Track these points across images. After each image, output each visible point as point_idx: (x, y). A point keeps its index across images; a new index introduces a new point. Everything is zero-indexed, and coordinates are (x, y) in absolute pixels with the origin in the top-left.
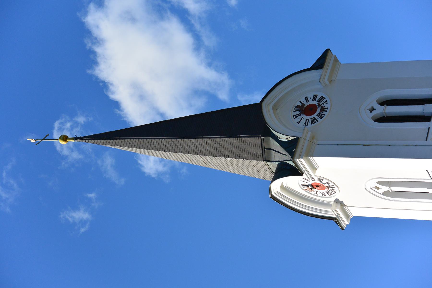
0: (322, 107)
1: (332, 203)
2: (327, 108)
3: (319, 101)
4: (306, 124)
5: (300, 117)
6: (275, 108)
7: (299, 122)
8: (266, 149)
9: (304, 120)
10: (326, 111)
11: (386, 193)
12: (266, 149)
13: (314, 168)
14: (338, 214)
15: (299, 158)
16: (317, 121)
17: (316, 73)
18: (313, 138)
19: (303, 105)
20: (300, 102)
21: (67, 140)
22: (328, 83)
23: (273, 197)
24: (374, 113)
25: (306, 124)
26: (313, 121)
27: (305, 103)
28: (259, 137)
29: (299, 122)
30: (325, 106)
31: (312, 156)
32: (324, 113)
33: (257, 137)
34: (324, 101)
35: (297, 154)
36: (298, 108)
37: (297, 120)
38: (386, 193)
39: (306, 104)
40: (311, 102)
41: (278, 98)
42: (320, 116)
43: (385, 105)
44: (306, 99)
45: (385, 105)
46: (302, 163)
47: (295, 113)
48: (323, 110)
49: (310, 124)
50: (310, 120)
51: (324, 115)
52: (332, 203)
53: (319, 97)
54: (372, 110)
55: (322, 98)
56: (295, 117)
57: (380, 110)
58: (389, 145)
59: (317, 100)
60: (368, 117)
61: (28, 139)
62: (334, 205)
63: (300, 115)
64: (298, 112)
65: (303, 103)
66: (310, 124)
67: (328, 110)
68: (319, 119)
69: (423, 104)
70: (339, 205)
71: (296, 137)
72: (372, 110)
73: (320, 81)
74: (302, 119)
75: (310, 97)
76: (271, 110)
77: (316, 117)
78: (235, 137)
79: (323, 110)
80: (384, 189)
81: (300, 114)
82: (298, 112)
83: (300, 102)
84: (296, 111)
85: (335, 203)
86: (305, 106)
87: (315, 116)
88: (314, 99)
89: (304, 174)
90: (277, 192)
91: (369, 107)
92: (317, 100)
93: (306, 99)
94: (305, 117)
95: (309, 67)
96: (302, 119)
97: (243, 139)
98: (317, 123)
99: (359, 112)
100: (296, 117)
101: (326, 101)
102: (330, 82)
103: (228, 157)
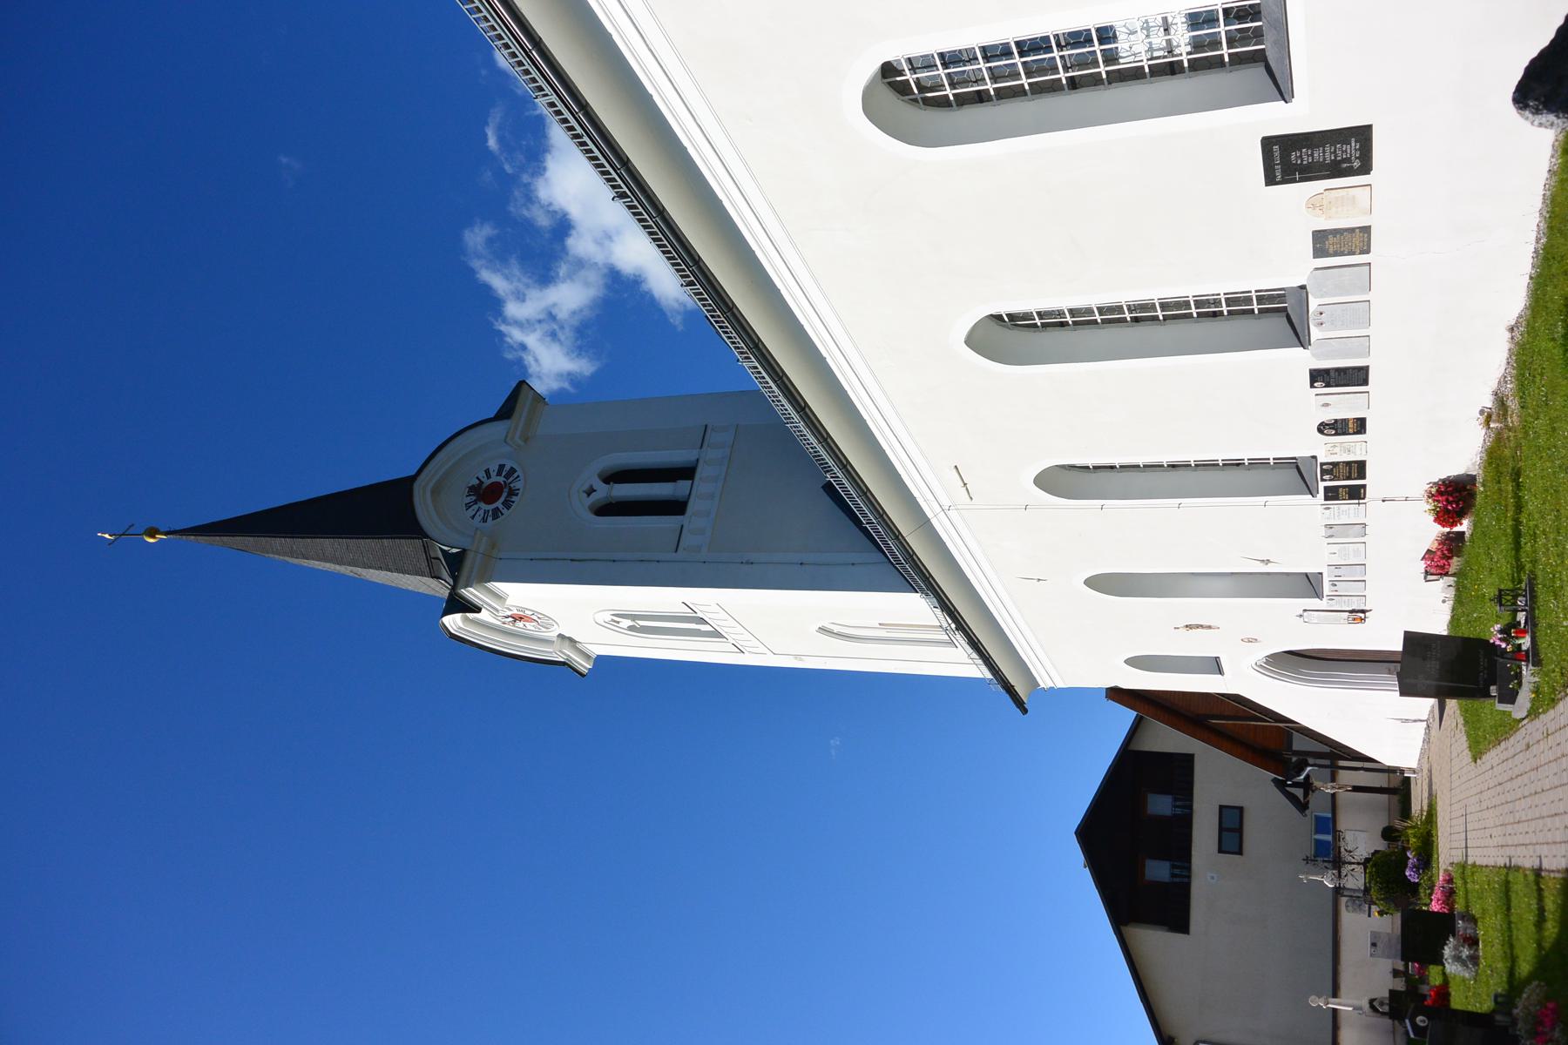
0: (510, 488)
1: (555, 639)
2: (518, 490)
3: (507, 476)
4: (484, 520)
5: (476, 507)
6: (436, 492)
7: (474, 516)
8: (434, 558)
9: (481, 513)
10: (517, 495)
11: (631, 628)
12: (434, 558)
13: (499, 597)
14: (568, 656)
15: (466, 587)
16: (502, 514)
17: (500, 428)
18: (493, 546)
19: (481, 483)
20: (478, 478)
21: (157, 536)
22: (522, 443)
23: (453, 636)
24: (594, 496)
25: (484, 520)
26: (496, 514)
27: (484, 480)
28: (419, 538)
29: (474, 516)
30: (517, 485)
31: (489, 582)
32: (514, 498)
33: (416, 538)
34: (515, 475)
35: (462, 580)
36: (473, 490)
37: (471, 512)
38: (631, 628)
39: (487, 482)
40: (494, 479)
41: (441, 473)
42: (507, 504)
43: (611, 483)
44: (487, 472)
45: (611, 483)
46: (471, 593)
47: (468, 500)
48: (512, 493)
49: (490, 519)
50: (491, 512)
51: (513, 502)
52: (555, 639)
53: (507, 468)
54: (591, 491)
55: (512, 471)
56: (468, 506)
57: (604, 492)
58: (614, 561)
59: (504, 474)
60: (582, 505)
61: (99, 534)
62: (558, 642)
63: (475, 502)
64: (474, 498)
65: (482, 479)
66: (490, 519)
67: (520, 492)
68: (505, 511)
69: (674, 480)
70: (567, 643)
71: (458, 550)
72: (591, 491)
73: (505, 442)
74: (478, 511)
75: (494, 468)
76: (428, 494)
77: (501, 507)
78: (386, 538)
79: (512, 493)
80: (626, 623)
81: (475, 500)
82: (474, 498)
83: (478, 478)
84: (470, 495)
85: (560, 640)
86: (484, 486)
87: (499, 504)
88: (499, 474)
89: (483, 610)
90: (460, 628)
91: (586, 487)
92: (504, 474)
93: (487, 472)
94: (484, 506)
95: (492, 416)
96: (478, 511)
97: (397, 541)
98: (502, 518)
99: (569, 496)
100: (470, 507)
101: (518, 476)
102: (526, 441)
103: (381, 568)
